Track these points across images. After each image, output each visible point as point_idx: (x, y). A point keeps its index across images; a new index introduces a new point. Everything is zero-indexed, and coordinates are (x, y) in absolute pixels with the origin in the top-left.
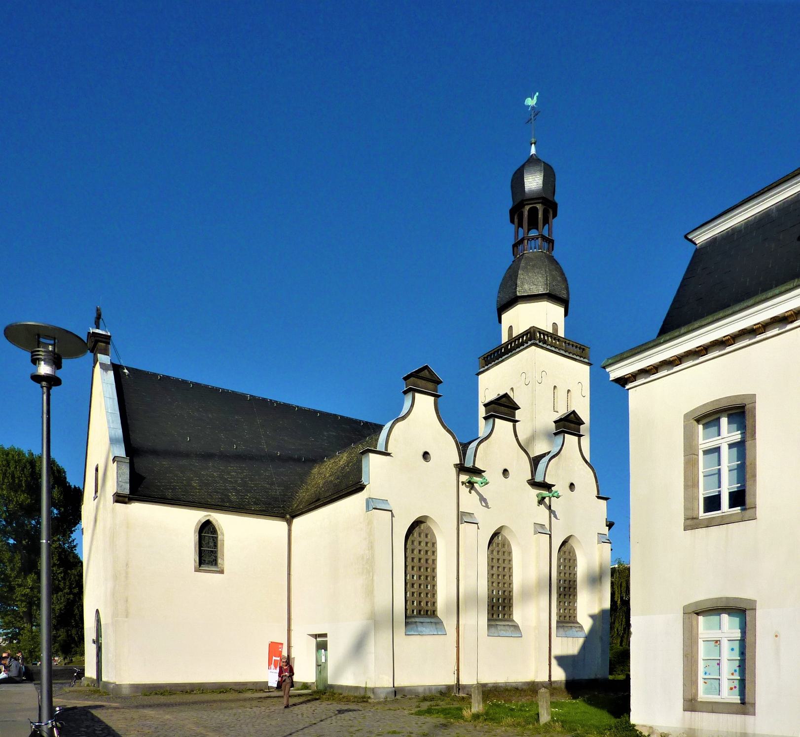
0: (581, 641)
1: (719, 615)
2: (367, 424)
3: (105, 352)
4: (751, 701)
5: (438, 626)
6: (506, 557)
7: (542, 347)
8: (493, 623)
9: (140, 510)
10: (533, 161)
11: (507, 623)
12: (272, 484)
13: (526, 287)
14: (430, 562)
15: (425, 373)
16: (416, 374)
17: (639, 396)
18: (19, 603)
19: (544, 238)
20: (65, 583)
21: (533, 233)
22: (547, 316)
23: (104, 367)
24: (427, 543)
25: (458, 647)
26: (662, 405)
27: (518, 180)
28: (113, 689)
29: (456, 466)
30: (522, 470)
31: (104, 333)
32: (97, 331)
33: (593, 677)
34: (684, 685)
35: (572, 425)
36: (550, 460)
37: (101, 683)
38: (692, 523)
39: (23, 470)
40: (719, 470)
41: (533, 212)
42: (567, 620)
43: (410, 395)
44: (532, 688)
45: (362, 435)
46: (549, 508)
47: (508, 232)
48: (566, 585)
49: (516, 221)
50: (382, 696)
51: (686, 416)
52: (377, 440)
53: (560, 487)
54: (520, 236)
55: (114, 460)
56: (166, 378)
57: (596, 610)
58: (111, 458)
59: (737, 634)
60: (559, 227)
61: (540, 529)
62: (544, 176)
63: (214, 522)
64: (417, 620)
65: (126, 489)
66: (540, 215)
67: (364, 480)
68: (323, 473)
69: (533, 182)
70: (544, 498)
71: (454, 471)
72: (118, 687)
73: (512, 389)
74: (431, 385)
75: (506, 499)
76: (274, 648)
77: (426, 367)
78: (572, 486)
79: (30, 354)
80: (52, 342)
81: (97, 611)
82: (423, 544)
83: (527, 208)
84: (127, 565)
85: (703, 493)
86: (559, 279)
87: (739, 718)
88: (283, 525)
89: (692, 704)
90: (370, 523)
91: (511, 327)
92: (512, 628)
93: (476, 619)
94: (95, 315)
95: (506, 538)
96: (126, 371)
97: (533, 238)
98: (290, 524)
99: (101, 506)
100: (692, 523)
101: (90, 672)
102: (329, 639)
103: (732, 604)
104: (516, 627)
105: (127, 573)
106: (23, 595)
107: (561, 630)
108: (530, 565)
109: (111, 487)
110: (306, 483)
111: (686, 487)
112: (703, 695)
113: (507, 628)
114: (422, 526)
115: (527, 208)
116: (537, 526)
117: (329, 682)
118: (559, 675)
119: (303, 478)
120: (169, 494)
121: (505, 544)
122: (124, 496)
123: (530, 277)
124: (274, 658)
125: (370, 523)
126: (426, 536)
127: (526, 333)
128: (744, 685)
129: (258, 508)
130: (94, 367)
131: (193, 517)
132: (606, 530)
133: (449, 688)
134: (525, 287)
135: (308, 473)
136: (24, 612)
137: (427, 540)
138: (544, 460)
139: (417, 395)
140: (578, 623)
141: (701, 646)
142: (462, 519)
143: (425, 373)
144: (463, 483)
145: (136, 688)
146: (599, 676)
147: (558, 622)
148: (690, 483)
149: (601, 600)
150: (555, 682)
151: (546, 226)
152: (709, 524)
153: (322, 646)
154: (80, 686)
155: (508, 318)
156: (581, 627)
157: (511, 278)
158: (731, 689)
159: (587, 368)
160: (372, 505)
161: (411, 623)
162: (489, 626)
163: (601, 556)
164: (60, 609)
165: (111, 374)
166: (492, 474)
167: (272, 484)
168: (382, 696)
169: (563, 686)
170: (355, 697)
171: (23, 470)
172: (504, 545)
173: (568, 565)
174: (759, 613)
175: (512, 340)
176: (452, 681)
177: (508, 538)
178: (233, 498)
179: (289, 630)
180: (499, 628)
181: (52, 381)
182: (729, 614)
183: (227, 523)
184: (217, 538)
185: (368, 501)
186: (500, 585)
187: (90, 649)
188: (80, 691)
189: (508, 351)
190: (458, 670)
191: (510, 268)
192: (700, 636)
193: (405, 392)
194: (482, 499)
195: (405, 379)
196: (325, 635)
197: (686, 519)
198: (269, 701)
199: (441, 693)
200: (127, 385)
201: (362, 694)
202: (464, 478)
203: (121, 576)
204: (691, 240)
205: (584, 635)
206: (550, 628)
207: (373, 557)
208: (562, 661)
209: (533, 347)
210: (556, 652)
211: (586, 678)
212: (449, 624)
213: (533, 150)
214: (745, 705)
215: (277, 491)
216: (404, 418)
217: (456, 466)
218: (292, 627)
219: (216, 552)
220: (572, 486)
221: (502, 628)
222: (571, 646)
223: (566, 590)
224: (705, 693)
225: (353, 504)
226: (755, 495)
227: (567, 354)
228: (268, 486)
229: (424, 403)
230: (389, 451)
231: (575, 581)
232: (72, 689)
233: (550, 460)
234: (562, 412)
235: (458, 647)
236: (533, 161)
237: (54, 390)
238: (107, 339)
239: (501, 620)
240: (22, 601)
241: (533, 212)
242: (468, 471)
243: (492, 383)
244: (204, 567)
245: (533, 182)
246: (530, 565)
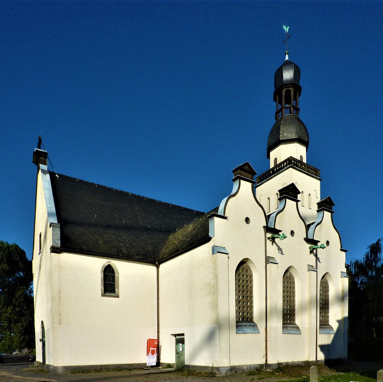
0: (332, 336)
5: (255, 328)
6: (291, 285)
7: (295, 169)
8: (285, 326)
9: (66, 257)
10: (288, 63)
11: (292, 326)
12: (146, 244)
13: (285, 134)
14: (249, 288)
15: (247, 167)
16: (241, 168)
18: (4, 321)
20: (28, 312)
22: (297, 151)
23: (44, 172)
24: (247, 276)
25: (266, 341)
27: (279, 74)
31: (43, 151)
32: (39, 150)
33: (338, 357)
35: (328, 206)
36: (316, 226)
37: (45, 365)
39: (4, 252)
41: (288, 92)
42: (324, 324)
43: (237, 182)
44: (307, 365)
46: (316, 255)
47: (273, 106)
48: (324, 303)
50: (224, 372)
54: (280, 107)
55: (50, 226)
56: (81, 181)
57: (340, 318)
58: (49, 225)
61: (311, 268)
62: (294, 71)
63: (113, 266)
64: (242, 324)
65: (58, 244)
67: (210, 234)
69: (288, 75)
71: (263, 231)
72: (55, 368)
74: (249, 175)
75: (293, 249)
76: (150, 343)
81: (42, 322)
82: (245, 276)
83: (285, 90)
84: (60, 292)
86: (303, 130)
88: (154, 268)
90: (215, 262)
92: (295, 329)
93: (276, 323)
94: (37, 141)
95: (291, 274)
96: (57, 176)
98: (158, 267)
99: (43, 257)
101: (39, 358)
102: (185, 337)
104: (298, 328)
105: (60, 297)
106: (6, 317)
107: (322, 330)
108: (305, 291)
109: (49, 243)
110: (166, 244)
113: (293, 329)
114: (244, 265)
115: (285, 90)
116: (310, 267)
117: (186, 363)
118: (321, 356)
119: (164, 241)
120: (85, 248)
122: (57, 248)
123: (287, 129)
124: (151, 349)
125: (215, 262)
126: (247, 271)
127: (286, 161)
129: (139, 257)
130: (38, 174)
131: (99, 263)
133: (261, 366)
134: (285, 134)
135: (166, 239)
136: (6, 326)
137: (247, 274)
138: (312, 227)
139: (242, 181)
140: (330, 325)
142: (268, 260)
143: (247, 167)
144: (269, 238)
145: (67, 368)
146: (342, 357)
147: (320, 325)
149: (343, 312)
150: (319, 361)
154: (33, 367)
155: (274, 154)
156: (332, 328)
157: (276, 130)
159: (319, 182)
160: (216, 250)
162: (283, 327)
163: (343, 285)
164: (26, 325)
165: (48, 176)
167: (146, 244)
168: (224, 372)
169: (323, 363)
170: (206, 373)
171: (4, 252)
172: (290, 278)
173: (324, 290)
176: (263, 362)
177: (293, 274)
178: (124, 251)
180: (289, 329)
183: (122, 268)
184: (114, 276)
185: (214, 248)
186: (288, 303)
188: (32, 371)
190: (266, 355)
191: (274, 125)
193: (234, 180)
194: (279, 249)
195: (234, 171)
196: (183, 335)
198: (151, 376)
199: (257, 369)
200: (58, 185)
201: (210, 371)
202: (269, 235)
203: (56, 299)
205: (334, 333)
206: (317, 328)
207: (217, 283)
208: (323, 348)
209: (291, 169)
210: (319, 343)
211: (335, 358)
212: (261, 326)
213: (287, 58)
215: (149, 248)
216: (234, 195)
218: (160, 330)
219: (114, 285)
221: (290, 328)
222: (326, 339)
223: (324, 306)
225: (203, 251)
227: (308, 173)
228: (144, 245)
230: (226, 216)
231: (328, 300)
232: (27, 369)
233: (316, 226)
235: (266, 341)
236: (288, 63)
238: (45, 155)
240: (5, 320)
241: (288, 92)
244: (107, 294)
245: (288, 75)
246: (305, 291)
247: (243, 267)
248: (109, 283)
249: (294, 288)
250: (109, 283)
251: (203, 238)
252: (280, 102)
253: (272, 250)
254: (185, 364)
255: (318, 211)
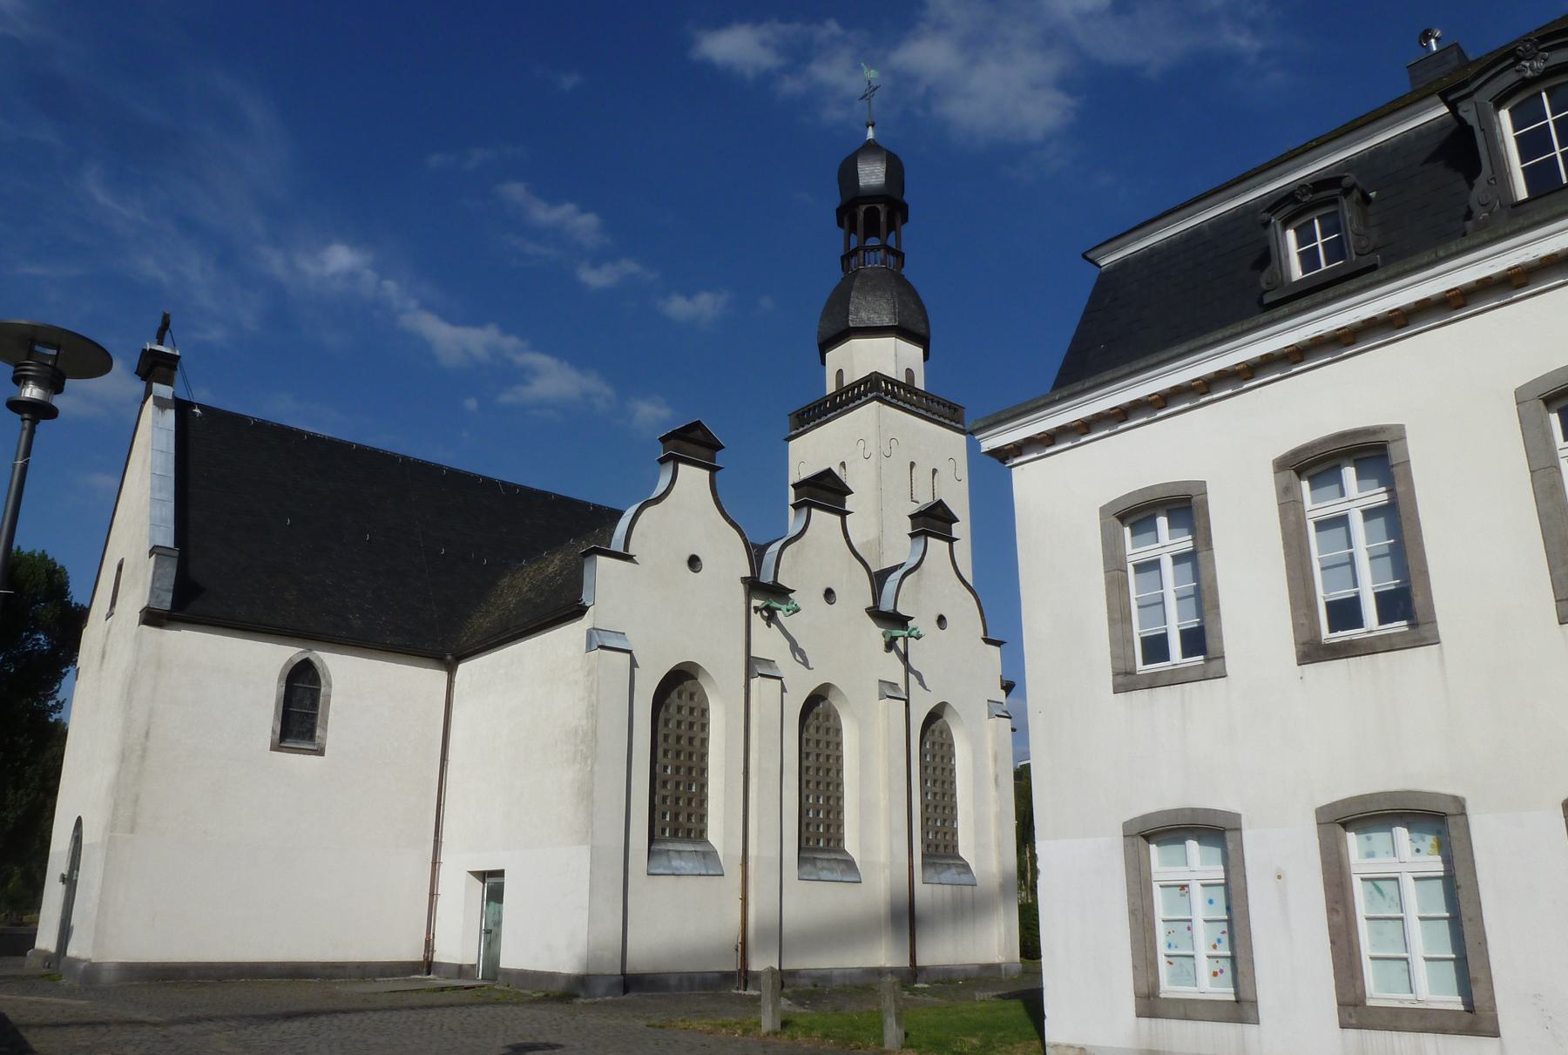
1: (1182, 842)
2: (598, 508)
3: (168, 381)
4: (1249, 996)
10: (871, 148)
11: (833, 856)
13: (863, 315)
14: (697, 742)
15: (698, 434)
17: (1027, 478)
19: (889, 250)
21: (873, 241)
22: (889, 356)
23: (161, 404)
25: (433, 895)
26: (1063, 496)
27: (848, 172)
28: (86, 971)
29: (744, 580)
30: (857, 592)
31: (169, 351)
34: (1135, 967)
38: (1126, 681)
40: (1351, 555)
41: (872, 215)
45: (586, 528)
46: (904, 658)
47: (835, 239)
49: (846, 223)
51: (1103, 510)
52: (612, 535)
53: (922, 622)
54: (854, 244)
59: (1217, 873)
60: (910, 236)
61: (888, 690)
63: (317, 663)
64: (670, 846)
65: (166, 602)
66: (883, 218)
67: (586, 598)
68: (521, 583)
69: (872, 174)
70: (896, 638)
71: (740, 590)
73: (843, 464)
74: (705, 451)
75: (844, 649)
77: (698, 424)
78: (941, 620)
79: (12, 369)
80: (54, 352)
82: (685, 712)
83: (863, 208)
85: (1138, 633)
87: (1229, 1030)
88: (441, 676)
89: (1150, 1004)
91: (840, 372)
92: (843, 866)
94: (159, 324)
97: (873, 249)
98: (451, 671)
100: (1126, 681)
101: (46, 940)
103: (1201, 821)
104: (850, 864)
105: (144, 750)
107: (930, 872)
111: (1112, 621)
112: (1169, 988)
113: (835, 865)
114: (688, 683)
121: (832, 718)
127: (864, 381)
128: (1239, 962)
132: (1000, 695)
133: (727, 977)
137: (693, 704)
139: (681, 466)
141: (1158, 893)
143: (698, 434)
144: (757, 609)
148: (1119, 616)
151: (893, 235)
152: (1152, 682)
153: (495, 895)
155: (834, 358)
158: (1215, 974)
161: (661, 852)
166: (806, 596)
172: (827, 717)
174: (1248, 835)
175: (842, 390)
179: (435, 863)
181: (40, 412)
182: (1200, 841)
185: (590, 634)
187: (53, 893)
189: (835, 407)
192: (1155, 877)
193: (662, 461)
195: (663, 440)
196: (500, 873)
197: (1116, 674)
200: (198, 436)
203: (135, 755)
204: (1091, 261)
209: (875, 403)
214: (1241, 1009)
217: (744, 580)
219: (314, 716)
220: (941, 620)
221: (825, 864)
224: (1171, 982)
225: (570, 636)
226: (1220, 638)
229: (693, 479)
234: (925, 500)
236: (871, 148)
237: (44, 426)
238: (171, 362)
239: (822, 850)
241: (872, 215)
242: (767, 593)
243: (809, 454)
247: (680, 684)
248: (300, 714)
249: (839, 745)
250: (300, 714)
251: (564, 606)
252: (853, 229)
253: (768, 642)
254: (503, 965)
255: (912, 536)
